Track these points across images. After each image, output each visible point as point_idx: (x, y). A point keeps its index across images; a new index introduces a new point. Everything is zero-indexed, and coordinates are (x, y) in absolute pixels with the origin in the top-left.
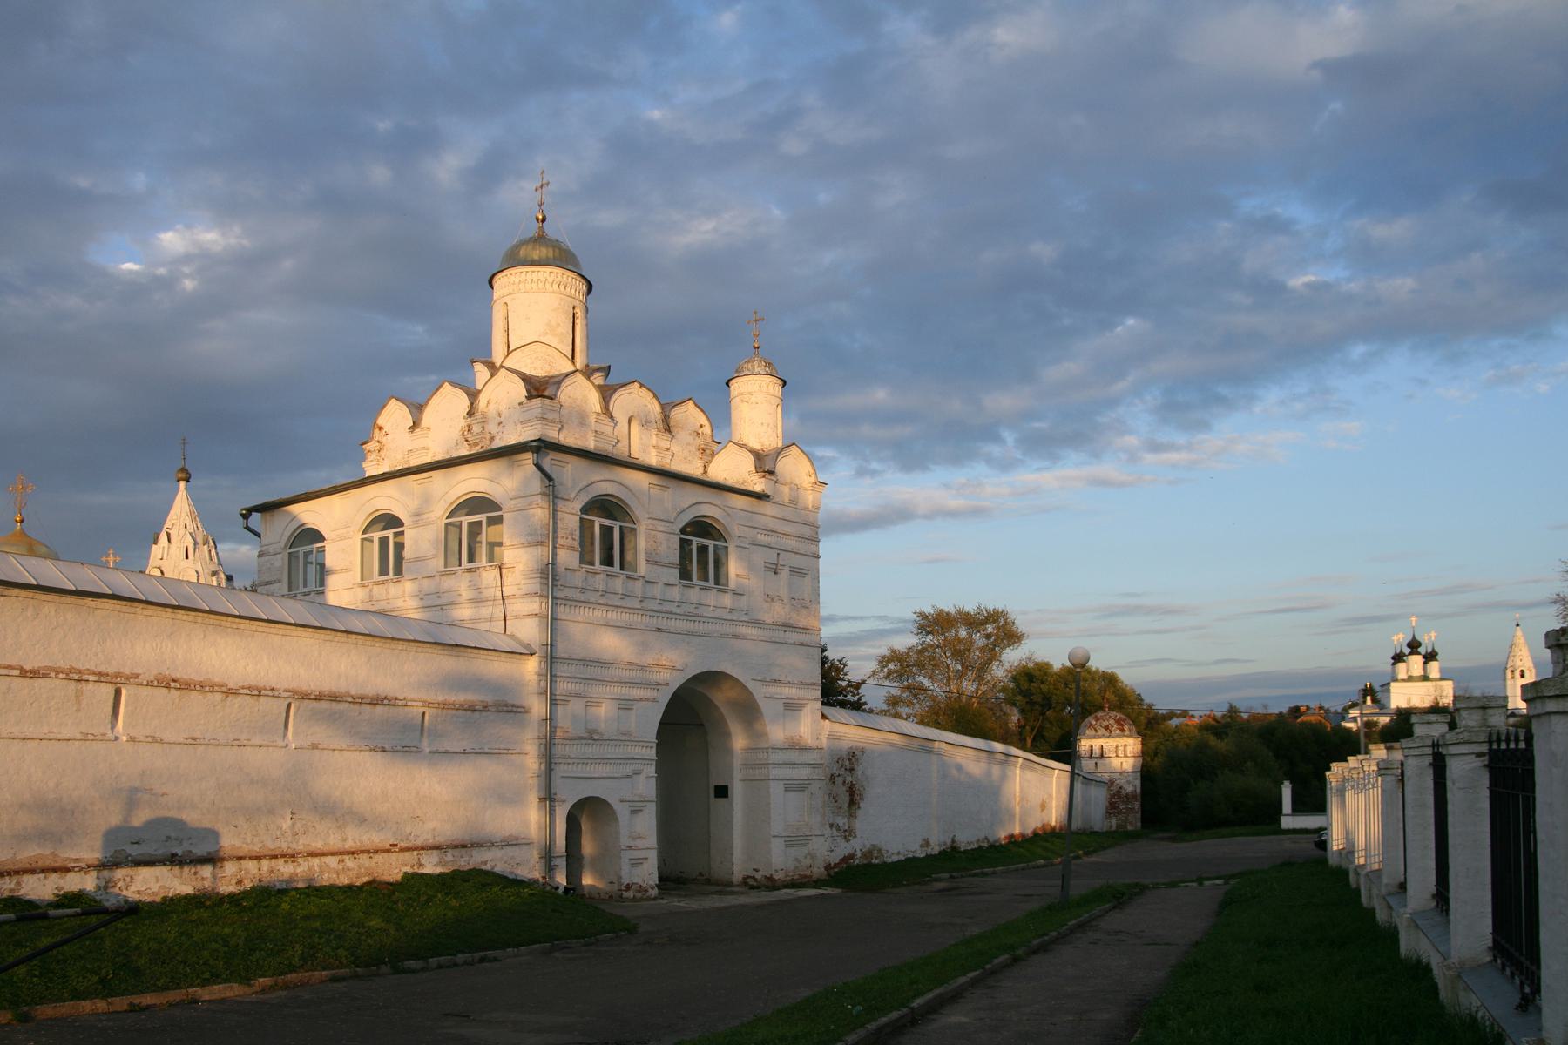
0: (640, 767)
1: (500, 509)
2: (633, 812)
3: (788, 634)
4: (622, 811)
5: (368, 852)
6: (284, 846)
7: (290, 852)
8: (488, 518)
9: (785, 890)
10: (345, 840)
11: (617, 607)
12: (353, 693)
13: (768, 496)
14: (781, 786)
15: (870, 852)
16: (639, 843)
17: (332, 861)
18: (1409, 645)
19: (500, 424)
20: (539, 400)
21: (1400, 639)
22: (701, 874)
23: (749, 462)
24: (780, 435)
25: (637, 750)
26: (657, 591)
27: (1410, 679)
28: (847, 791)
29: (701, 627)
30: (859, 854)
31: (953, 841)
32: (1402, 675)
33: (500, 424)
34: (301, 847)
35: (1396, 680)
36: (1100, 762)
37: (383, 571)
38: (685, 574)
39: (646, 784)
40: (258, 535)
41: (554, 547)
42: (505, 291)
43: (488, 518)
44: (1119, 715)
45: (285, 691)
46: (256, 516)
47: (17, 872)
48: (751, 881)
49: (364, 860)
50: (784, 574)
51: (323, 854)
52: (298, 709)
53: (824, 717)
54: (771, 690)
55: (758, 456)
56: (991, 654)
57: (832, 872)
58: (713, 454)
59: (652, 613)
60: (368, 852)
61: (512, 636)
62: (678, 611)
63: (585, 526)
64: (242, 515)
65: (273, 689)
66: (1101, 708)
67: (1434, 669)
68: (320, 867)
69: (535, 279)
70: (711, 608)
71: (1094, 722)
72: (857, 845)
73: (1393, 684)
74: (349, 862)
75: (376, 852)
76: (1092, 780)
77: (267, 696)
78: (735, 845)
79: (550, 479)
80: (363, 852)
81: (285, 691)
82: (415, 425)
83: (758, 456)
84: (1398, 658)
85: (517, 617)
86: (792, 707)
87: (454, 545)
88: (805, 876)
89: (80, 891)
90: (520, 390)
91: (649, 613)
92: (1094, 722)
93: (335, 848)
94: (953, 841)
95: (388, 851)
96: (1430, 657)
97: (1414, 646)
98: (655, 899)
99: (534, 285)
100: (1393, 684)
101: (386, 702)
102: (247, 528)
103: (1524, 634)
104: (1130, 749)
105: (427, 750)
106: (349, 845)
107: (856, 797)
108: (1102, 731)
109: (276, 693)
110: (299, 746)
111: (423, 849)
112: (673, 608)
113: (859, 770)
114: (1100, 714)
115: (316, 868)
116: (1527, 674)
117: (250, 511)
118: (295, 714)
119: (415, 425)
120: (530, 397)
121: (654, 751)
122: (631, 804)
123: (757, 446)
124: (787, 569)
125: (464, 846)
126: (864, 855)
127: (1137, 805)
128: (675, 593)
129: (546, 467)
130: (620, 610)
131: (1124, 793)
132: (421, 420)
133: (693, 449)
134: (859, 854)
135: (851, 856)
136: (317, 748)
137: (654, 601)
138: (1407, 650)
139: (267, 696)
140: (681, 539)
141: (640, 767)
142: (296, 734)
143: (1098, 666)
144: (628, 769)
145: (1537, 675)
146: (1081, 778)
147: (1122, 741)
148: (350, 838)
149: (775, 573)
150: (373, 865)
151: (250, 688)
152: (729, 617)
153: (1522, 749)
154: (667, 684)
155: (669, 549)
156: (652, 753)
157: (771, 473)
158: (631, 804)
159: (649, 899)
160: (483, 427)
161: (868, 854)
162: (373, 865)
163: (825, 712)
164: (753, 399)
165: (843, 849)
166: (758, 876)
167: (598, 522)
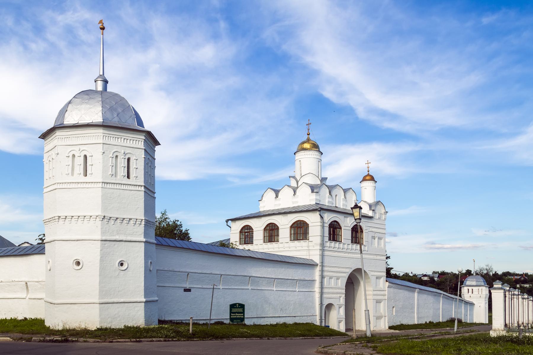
0: (341, 295)
3: (349, 255)
11: (336, 251)
13: (373, 217)
24: (297, 163)
26: (346, 246)
28: (277, 323)
39: (342, 301)
40: (230, 227)
46: (230, 221)
50: (376, 239)
53: (387, 281)
59: (345, 253)
64: (226, 221)
70: (337, 248)
76: (468, 303)
82: (277, 196)
86: (378, 278)
91: (344, 252)
99: (312, 156)
102: (227, 225)
105: (297, 291)
116: (467, 291)
117: (228, 220)
122: (339, 305)
128: (350, 246)
130: (337, 252)
137: (365, 251)
141: (341, 295)
143: (460, 270)
144: (339, 295)
145: (101, 322)
146: (464, 302)
149: (374, 239)
156: (344, 291)
158: (339, 305)
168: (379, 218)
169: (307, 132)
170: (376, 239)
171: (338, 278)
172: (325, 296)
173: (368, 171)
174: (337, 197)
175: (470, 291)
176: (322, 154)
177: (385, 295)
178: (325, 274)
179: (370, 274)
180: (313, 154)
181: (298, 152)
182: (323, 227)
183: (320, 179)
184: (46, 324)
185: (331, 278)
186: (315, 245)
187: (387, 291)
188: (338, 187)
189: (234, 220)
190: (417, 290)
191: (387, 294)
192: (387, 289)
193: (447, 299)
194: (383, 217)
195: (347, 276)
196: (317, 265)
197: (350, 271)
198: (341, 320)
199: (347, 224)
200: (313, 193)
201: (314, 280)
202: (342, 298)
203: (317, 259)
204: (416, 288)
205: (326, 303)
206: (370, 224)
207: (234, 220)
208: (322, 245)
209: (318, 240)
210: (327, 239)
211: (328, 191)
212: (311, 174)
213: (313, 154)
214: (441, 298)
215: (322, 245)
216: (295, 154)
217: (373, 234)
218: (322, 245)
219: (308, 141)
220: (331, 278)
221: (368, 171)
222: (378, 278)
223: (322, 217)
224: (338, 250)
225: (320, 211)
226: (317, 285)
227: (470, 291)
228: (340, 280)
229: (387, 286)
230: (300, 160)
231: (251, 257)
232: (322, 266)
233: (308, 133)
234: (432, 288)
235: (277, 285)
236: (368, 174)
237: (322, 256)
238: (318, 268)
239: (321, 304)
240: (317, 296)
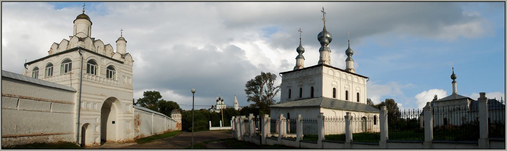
1: (71, 61)
5: (35, 136)
6: (14, 134)
7: (15, 136)
8: (69, 63)
9: (126, 144)
10: (30, 132)
12: (35, 98)
15: (142, 135)
16: (97, 133)
17: (26, 138)
18: (219, 99)
20: (81, 42)
21: (217, 98)
22: (109, 140)
23: (120, 56)
25: (97, 113)
26: (102, 79)
27: (219, 104)
29: (110, 87)
30: (140, 135)
31: (423, 144)
32: (218, 104)
34: (18, 134)
35: (217, 105)
36: (175, 118)
37: (49, 75)
38: (107, 77)
39: (99, 121)
41: (82, 69)
42: (76, 23)
43: (69, 63)
44: (178, 110)
45: (18, 96)
47: (47, 135)
48: (119, 142)
49: (34, 138)
50: (126, 78)
51: (24, 136)
52: (21, 100)
53: (133, 107)
54: (123, 101)
55: (122, 55)
56: (156, 99)
57: (135, 139)
58: (113, 55)
60: (35, 136)
61: (72, 88)
62: (106, 84)
63: (88, 66)
65: (15, 95)
66: (175, 109)
67: (223, 103)
68: (22, 139)
72: (139, 134)
73: (217, 105)
74: (30, 138)
75: (37, 135)
77: (13, 97)
80: (34, 136)
81: (18, 96)
82: (58, 47)
83: (122, 55)
84: (217, 101)
87: (62, 70)
88: (130, 140)
89: (391, 99)
90: (78, 40)
93: (27, 135)
94: (423, 144)
95: (40, 135)
96: (222, 101)
97: (220, 99)
98: (100, 146)
100: (217, 105)
101: (42, 100)
103: (236, 97)
104: (180, 116)
105: (52, 112)
106: (31, 134)
107: (139, 124)
108: (175, 113)
109: (15, 96)
110: (20, 109)
111: (49, 135)
112: (105, 83)
113: (140, 118)
114: (175, 109)
115: (22, 139)
118: (20, 102)
119: (58, 47)
120: (79, 41)
123: (121, 53)
125: (59, 134)
126: (141, 136)
127: (181, 126)
128: (106, 80)
129: (81, 53)
131: (254, 117)
132: (59, 46)
133: (110, 53)
134: (140, 135)
135: (138, 136)
136: (25, 110)
138: (219, 100)
139: (13, 97)
140: (107, 70)
142: (19, 107)
144: (95, 117)
147: (179, 114)
148: (31, 132)
150: (36, 138)
151: (9, 95)
154: (103, 99)
155: (105, 72)
157: (124, 58)
159: (98, 146)
161: (141, 136)
162: (36, 138)
164: (121, 44)
165: (137, 135)
166: (121, 140)
167: (91, 65)
168: (128, 64)
170: (126, 78)
171: (94, 104)
173: (122, 35)
174: (99, 48)
175: (174, 116)
184: (475, 100)
187: (134, 114)
189: (29, 64)
190: (153, 114)
191: (374, 114)
193: (167, 119)
194: (131, 64)
195: (103, 102)
196: (76, 92)
197: (105, 98)
198: (97, 136)
199: (102, 64)
202: (98, 119)
203: (76, 87)
204: (153, 113)
205: (83, 123)
206: (121, 67)
207: (29, 64)
209: (78, 71)
210: (85, 72)
211: (91, 42)
217: (124, 74)
220: (88, 103)
221: (122, 35)
222: (127, 104)
223: (81, 54)
224: (91, 81)
226: (75, 107)
227: (174, 116)
228: (96, 105)
229: (134, 111)
235: (23, 105)
236: (83, 13)
239: (79, 123)
240: (75, 116)
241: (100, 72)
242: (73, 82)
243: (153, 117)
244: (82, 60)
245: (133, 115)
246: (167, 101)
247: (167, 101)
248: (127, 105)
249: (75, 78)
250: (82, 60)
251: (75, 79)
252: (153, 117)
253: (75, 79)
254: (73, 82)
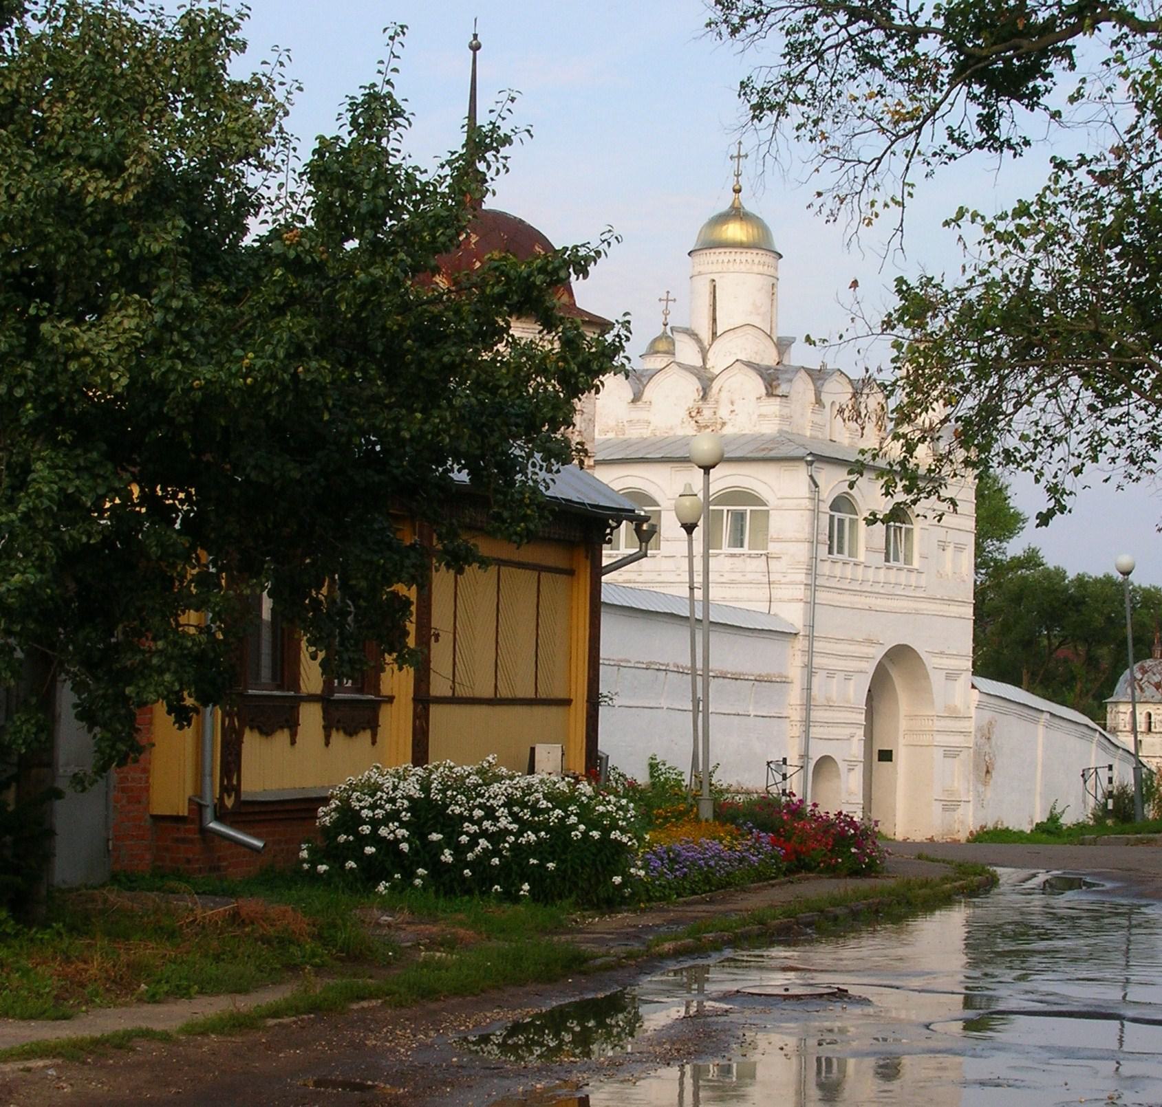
0: (853, 731)
2: (850, 770)
4: (843, 766)
14: (940, 752)
19: (732, 411)
33: (732, 411)
50: (950, 550)
53: (973, 687)
69: (750, 260)
71: (1139, 676)
78: (897, 806)
79: (817, 486)
85: (781, 601)
86: (951, 676)
92: (1139, 676)
113: (993, 738)
119: (636, 399)
121: (863, 716)
124: (952, 545)
152: (913, 594)
153: (446, 863)
156: (861, 718)
160: (715, 412)
163: (976, 684)
169: (732, 182)
172: (815, 731)
176: (781, 256)
177: (911, 731)
178: (817, 661)
179: (930, 662)
180: (756, 261)
181: (701, 252)
182: (816, 512)
183: (775, 340)
185: (831, 674)
186: (789, 571)
187: (973, 719)
188: (836, 376)
192: (973, 712)
200: (772, 400)
201: (785, 681)
202: (855, 740)
203: (792, 615)
205: (815, 756)
208: (812, 570)
209: (801, 551)
212: (750, 328)
213: (756, 261)
214: (1094, 746)
215: (811, 570)
216: (693, 254)
218: (811, 570)
219: (737, 214)
220: (831, 674)
222: (951, 676)
225: (810, 463)
226: (795, 695)
229: (974, 704)
230: (712, 277)
231: (632, 608)
232: (811, 638)
233: (737, 187)
234: (1072, 711)
237: (811, 605)
238: (800, 643)
241: (867, 542)
242: (778, 593)
243: (1040, 740)
244: (807, 732)
245: (970, 726)
246: (1071, 575)
247: (1071, 575)
248: (908, 151)
249: (789, 578)
250: (807, 732)
251: (792, 583)
252: (1040, 740)
253: (792, 583)
254: (778, 593)
